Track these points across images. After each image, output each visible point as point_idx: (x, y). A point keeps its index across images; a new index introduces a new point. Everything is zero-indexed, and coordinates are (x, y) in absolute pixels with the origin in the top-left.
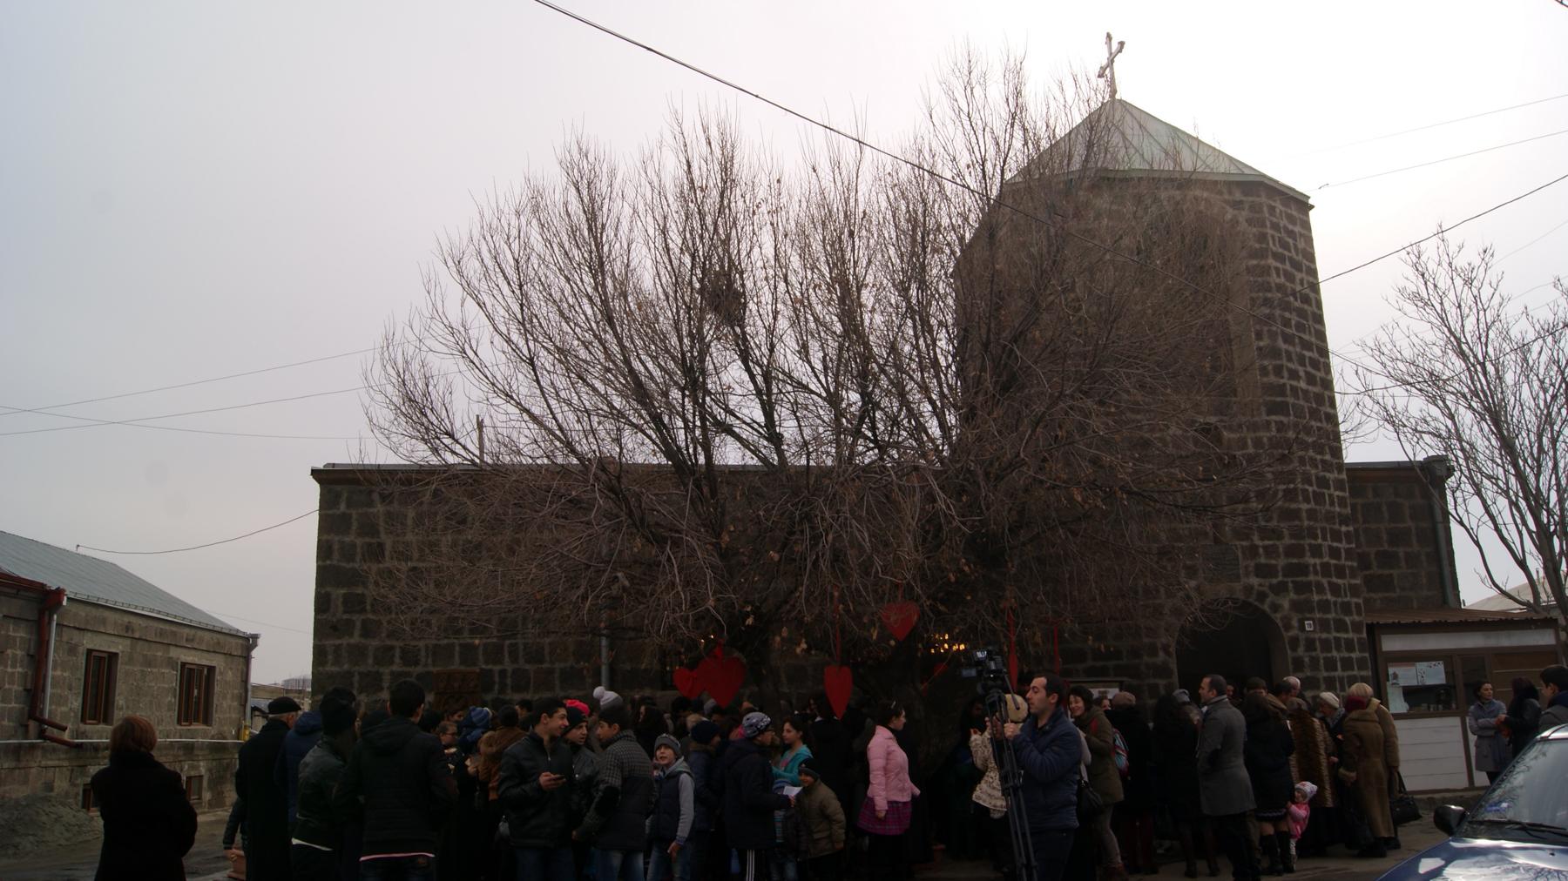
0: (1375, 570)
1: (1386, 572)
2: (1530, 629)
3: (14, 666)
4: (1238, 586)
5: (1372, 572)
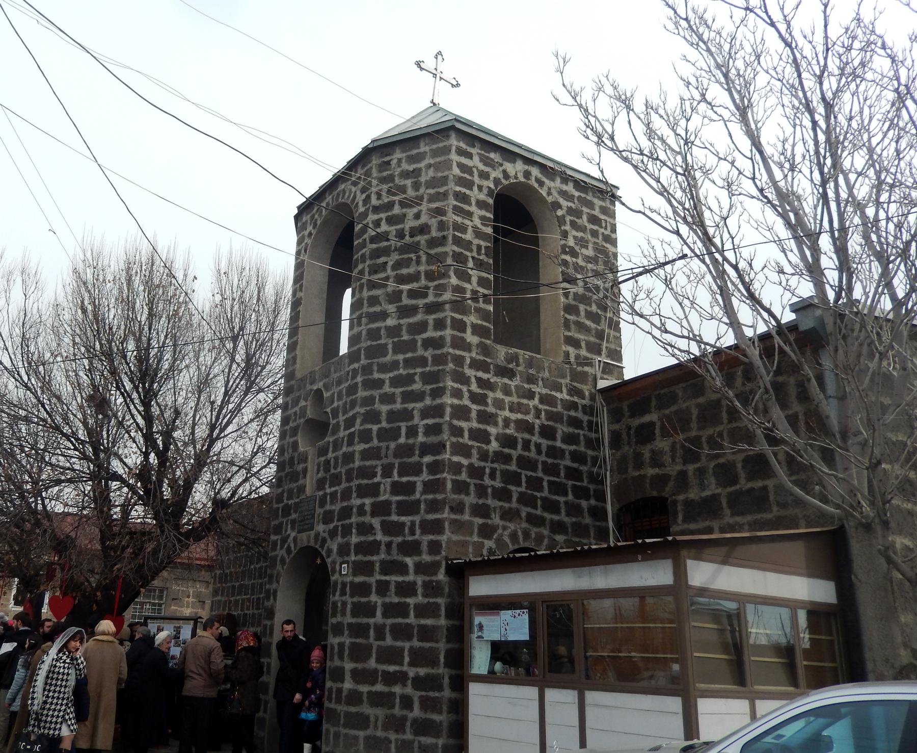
0: (744, 484)
1: (759, 484)
2: (637, 561)
3: (341, 645)
4: (312, 533)
5: (738, 487)
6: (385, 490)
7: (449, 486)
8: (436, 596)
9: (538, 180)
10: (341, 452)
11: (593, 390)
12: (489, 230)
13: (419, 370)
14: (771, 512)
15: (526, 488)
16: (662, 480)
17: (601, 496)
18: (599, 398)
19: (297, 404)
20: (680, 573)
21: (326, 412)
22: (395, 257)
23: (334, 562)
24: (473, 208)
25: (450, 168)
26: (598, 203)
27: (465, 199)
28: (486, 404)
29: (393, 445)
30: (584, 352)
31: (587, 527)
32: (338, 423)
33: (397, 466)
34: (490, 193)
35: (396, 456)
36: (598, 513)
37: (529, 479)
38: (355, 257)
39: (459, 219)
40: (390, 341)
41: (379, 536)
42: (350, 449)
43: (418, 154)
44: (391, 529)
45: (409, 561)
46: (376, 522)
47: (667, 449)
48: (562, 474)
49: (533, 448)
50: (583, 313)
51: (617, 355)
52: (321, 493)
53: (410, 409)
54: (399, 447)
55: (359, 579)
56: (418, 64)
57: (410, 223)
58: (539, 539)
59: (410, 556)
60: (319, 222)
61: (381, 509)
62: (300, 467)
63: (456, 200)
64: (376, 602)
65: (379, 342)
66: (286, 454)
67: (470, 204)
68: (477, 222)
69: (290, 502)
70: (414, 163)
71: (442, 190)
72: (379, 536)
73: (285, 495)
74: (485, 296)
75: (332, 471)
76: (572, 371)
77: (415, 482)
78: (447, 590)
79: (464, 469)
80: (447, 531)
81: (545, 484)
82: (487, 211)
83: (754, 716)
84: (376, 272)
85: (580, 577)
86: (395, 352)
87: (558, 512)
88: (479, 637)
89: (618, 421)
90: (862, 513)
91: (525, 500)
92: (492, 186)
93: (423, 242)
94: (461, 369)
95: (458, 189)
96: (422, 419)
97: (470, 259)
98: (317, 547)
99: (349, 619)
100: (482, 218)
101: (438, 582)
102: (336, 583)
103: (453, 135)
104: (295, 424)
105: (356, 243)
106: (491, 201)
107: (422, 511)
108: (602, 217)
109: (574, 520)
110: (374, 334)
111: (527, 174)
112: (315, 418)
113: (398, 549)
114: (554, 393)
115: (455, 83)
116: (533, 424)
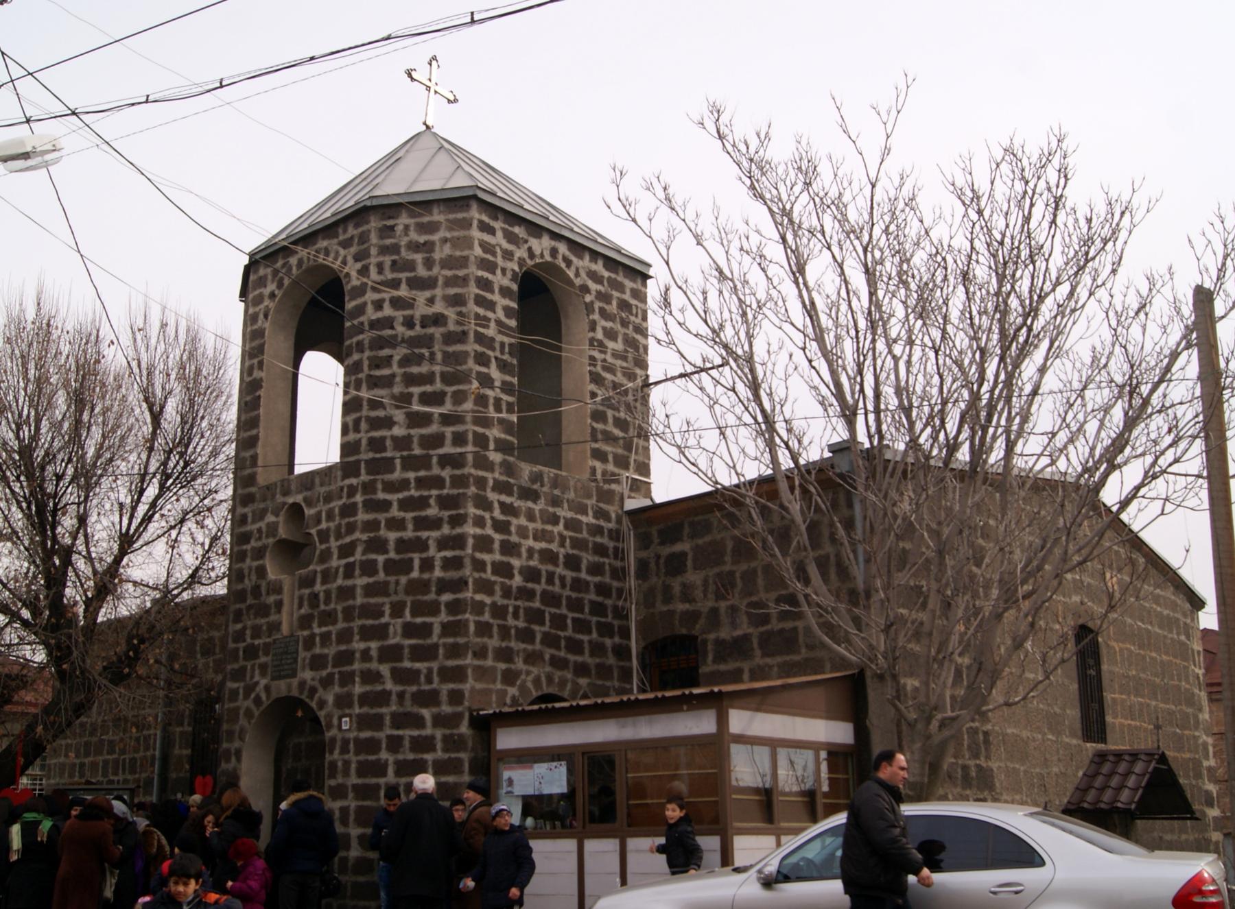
2: (682, 710)
3: (344, 811)
5: (769, 627)
6: (395, 633)
7: (472, 628)
8: (458, 751)
9: (565, 259)
10: (335, 585)
11: (620, 512)
12: (513, 323)
13: (434, 492)
14: (800, 653)
15: (551, 627)
16: (693, 616)
17: (625, 633)
18: (625, 520)
19: (262, 518)
20: (722, 721)
21: (310, 534)
22: (399, 353)
23: (329, 716)
24: (496, 297)
25: (471, 247)
26: (629, 284)
27: (485, 285)
28: (509, 533)
29: (403, 580)
30: (611, 467)
31: (610, 668)
32: (329, 549)
33: (409, 604)
34: (514, 279)
35: (407, 592)
36: (622, 652)
37: (554, 617)
38: (347, 343)
39: (481, 311)
40: (398, 455)
41: (389, 685)
42: (349, 582)
43: (430, 223)
44: (402, 676)
45: (426, 713)
46: (385, 669)
47: (699, 582)
48: (587, 610)
49: (557, 581)
50: (610, 420)
51: (644, 469)
52: (306, 633)
53: (424, 538)
55: (366, 734)
57: (421, 310)
58: (563, 683)
61: (390, 654)
62: (272, 599)
63: (478, 287)
65: (384, 455)
66: (246, 581)
67: (492, 292)
68: (501, 314)
69: (257, 642)
70: (426, 233)
71: (461, 273)
72: (389, 685)
73: (248, 632)
74: (509, 404)
75: (322, 607)
76: (599, 489)
77: (431, 624)
78: (470, 744)
79: (487, 609)
80: (470, 680)
81: (569, 622)
82: (511, 299)
83: (779, 844)
84: (378, 367)
85: (623, 727)
86: (405, 468)
87: (581, 652)
88: (508, 793)
89: (647, 548)
90: (877, 665)
91: (550, 640)
92: (516, 268)
93: (438, 336)
94: (483, 493)
95: (480, 273)
96: (440, 550)
97: (493, 360)
98: (303, 697)
99: (354, 780)
100: (507, 309)
101: (460, 735)
102: (333, 740)
103: (474, 206)
104: (260, 544)
105: (348, 324)
106: (515, 287)
107: (441, 657)
108: (633, 302)
109: (598, 660)
110: (377, 445)
111: (554, 252)
112: (290, 538)
114: (579, 517)
115: (452, 98)
116: (558, 554)
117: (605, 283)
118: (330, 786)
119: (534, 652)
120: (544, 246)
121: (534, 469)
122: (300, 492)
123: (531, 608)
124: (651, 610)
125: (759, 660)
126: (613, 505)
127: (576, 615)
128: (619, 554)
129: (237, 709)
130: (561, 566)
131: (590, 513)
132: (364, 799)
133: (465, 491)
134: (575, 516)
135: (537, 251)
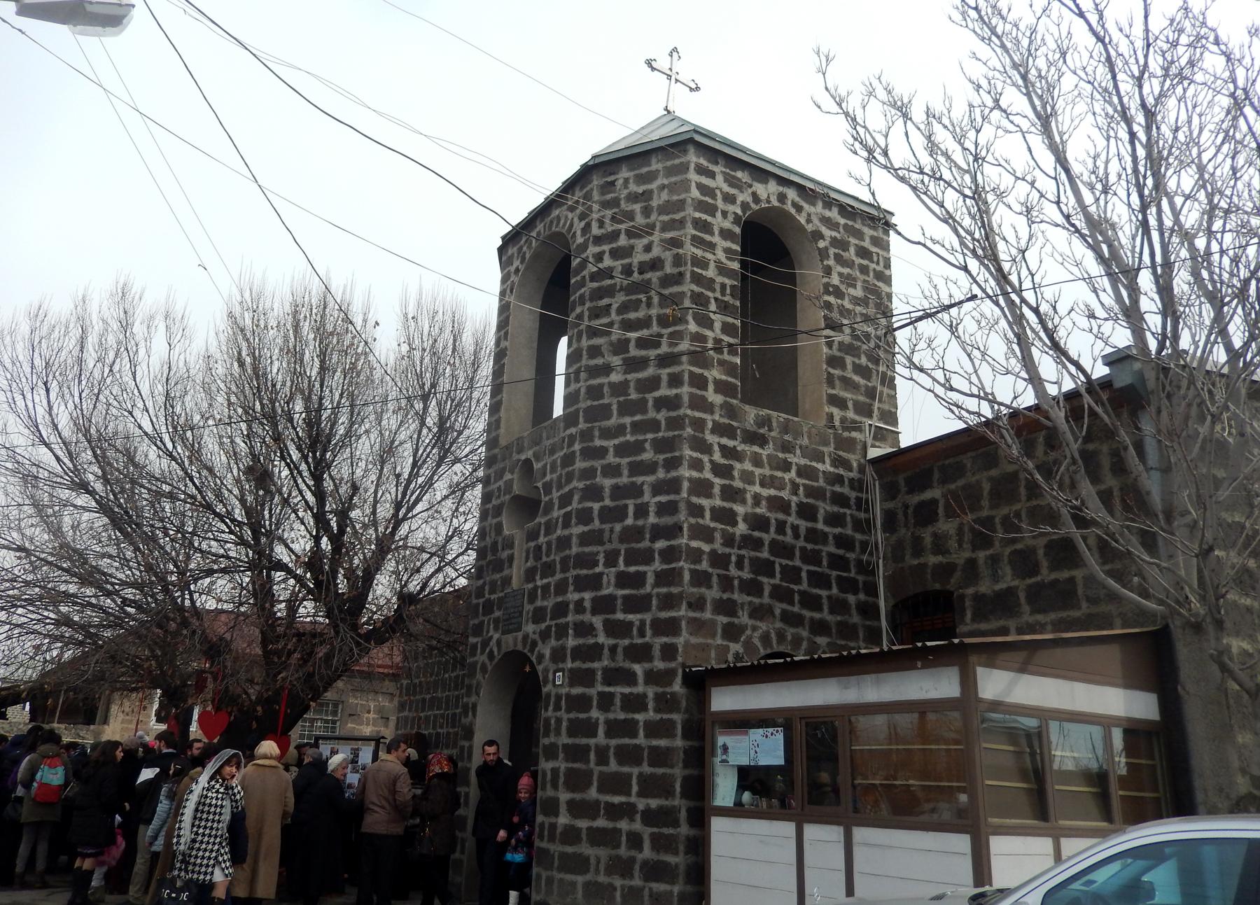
0: (1046, 574)
1: (1065, 574)
2: (915, 668)
3: (555, 771)
4: (520, 635)
7: (687, 576)
8: (671, 712)
9: (794, 205)
10: (555, 536)
11: (862, 461)
12: (735, 266)
13: (650, 436)
14: (1080, 608)
15: (781, 580)
16: (947, 570)
17: (872, 590)
19: (501, 478)
20: (968, 682)
21: (537, 487)
22: (621, 298)
23: (546, 670)
24: (716, 239)
25: (688, 190)
26: (868, 232)
27: (705, 227)
28: (732, 478)
29: (618, 527)
30: (851, 414)
32: (551, 500)
33: (623, 552)
34: (737, 219)
35: (621, 541)
36: (869, 611)
38: (572, 298)
39: (699, 253)
40: (615, 401)
41: (601, 639)
42: (566, 532)
44: (615, 629)
45: (638, 668)
46: (598, 621)
47: (952, 532)
48: (825, 563)
49: (789, 531)
50: (849, 367)
52: (530, 586)
53: (639, 483)
54: (626, 530)
56: (649, 63)
57: (639, 257)
58: (797, 641)
59: (639, 662)
60: (528, 256)
61: (603, 605)
63: (695, 228)
64: (598, 719)
65: (601, 402)
66: (488, 538)
67: (712, 234)
68: (721, 256)
69: (493, 597)
70: (644, 183)
71: (677, 216)
72: (601, 639)
73: (487, 588)
75: (544, 559)
77: (645, 573)
78: (684, 704)
79: (705, 557)
80: (684, 633)
81: (804, 575)
84: (597, 316)
85: (846, 688)
86: (622, 413)
87: (819, 608)
88: (723, 761)
89: (893, 498)
90: (1190, 610)
91: (778, 593)
92: (739, 212)
93: (654, 280)
94: (701, 435)
95: (697, 215)
96: (654, 496)
97: (713, 301)
98: (526, 651)
99: (565, 739)
100: (727, 251)
101: (673, 694)
102: (548, 695)
103: (691, 150)
104: (499, 501)
106: (738, 230)
107: (654, 608)
108: (874, 249)
109: (839, 618)
111: (782, 198)
113: (625, 655)
114: (814, 464)
115: (694, 86)
117: (841, 229)
118: (544, 745)
119: (761, 605)
120: (770, 191)
121: (761, 413)
122: (530, 448)
123: (758, 559)
124: (900, 565)
125: (1027, 617)
126: (854, 454)
127: (812, 568)
128: (861, 505)
129: (476, 662)
130: (794, 514)
131: (827, 460)
132: (574, 761)
133: (680, 432)
134: (809, 463)
135: (763, 195)
